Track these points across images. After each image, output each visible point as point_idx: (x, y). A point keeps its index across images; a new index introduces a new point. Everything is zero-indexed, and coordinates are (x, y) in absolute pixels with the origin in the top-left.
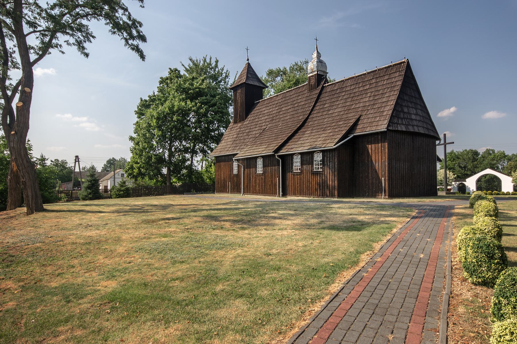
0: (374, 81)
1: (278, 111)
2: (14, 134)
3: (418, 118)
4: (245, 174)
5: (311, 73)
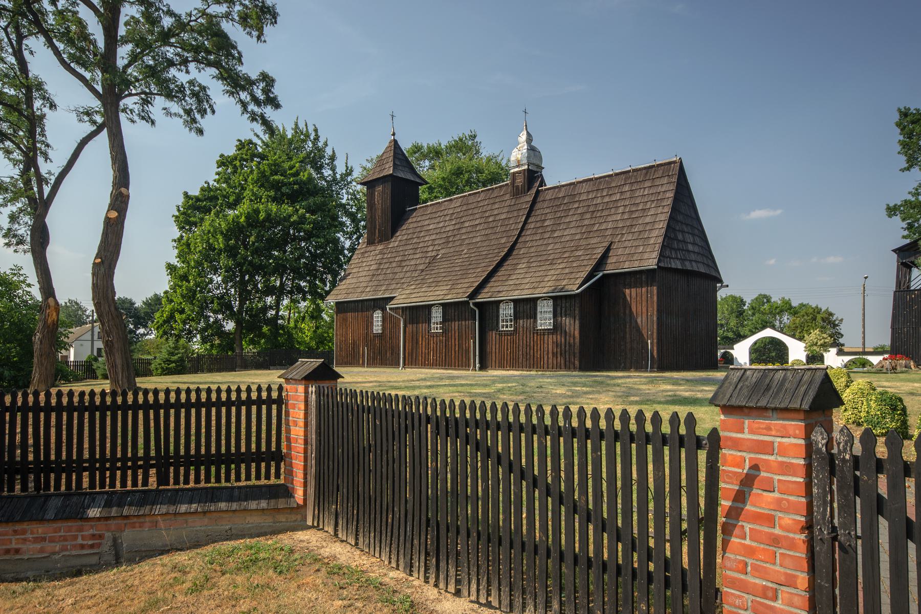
0: (627, 188)
1: (457, 227)
2: (100, 263)
3: (696, 249)
4: (407, 333)
5: (518, 166)
